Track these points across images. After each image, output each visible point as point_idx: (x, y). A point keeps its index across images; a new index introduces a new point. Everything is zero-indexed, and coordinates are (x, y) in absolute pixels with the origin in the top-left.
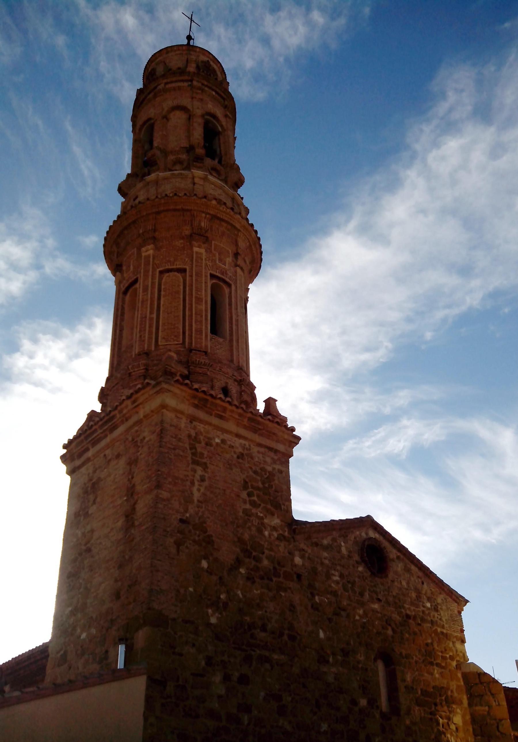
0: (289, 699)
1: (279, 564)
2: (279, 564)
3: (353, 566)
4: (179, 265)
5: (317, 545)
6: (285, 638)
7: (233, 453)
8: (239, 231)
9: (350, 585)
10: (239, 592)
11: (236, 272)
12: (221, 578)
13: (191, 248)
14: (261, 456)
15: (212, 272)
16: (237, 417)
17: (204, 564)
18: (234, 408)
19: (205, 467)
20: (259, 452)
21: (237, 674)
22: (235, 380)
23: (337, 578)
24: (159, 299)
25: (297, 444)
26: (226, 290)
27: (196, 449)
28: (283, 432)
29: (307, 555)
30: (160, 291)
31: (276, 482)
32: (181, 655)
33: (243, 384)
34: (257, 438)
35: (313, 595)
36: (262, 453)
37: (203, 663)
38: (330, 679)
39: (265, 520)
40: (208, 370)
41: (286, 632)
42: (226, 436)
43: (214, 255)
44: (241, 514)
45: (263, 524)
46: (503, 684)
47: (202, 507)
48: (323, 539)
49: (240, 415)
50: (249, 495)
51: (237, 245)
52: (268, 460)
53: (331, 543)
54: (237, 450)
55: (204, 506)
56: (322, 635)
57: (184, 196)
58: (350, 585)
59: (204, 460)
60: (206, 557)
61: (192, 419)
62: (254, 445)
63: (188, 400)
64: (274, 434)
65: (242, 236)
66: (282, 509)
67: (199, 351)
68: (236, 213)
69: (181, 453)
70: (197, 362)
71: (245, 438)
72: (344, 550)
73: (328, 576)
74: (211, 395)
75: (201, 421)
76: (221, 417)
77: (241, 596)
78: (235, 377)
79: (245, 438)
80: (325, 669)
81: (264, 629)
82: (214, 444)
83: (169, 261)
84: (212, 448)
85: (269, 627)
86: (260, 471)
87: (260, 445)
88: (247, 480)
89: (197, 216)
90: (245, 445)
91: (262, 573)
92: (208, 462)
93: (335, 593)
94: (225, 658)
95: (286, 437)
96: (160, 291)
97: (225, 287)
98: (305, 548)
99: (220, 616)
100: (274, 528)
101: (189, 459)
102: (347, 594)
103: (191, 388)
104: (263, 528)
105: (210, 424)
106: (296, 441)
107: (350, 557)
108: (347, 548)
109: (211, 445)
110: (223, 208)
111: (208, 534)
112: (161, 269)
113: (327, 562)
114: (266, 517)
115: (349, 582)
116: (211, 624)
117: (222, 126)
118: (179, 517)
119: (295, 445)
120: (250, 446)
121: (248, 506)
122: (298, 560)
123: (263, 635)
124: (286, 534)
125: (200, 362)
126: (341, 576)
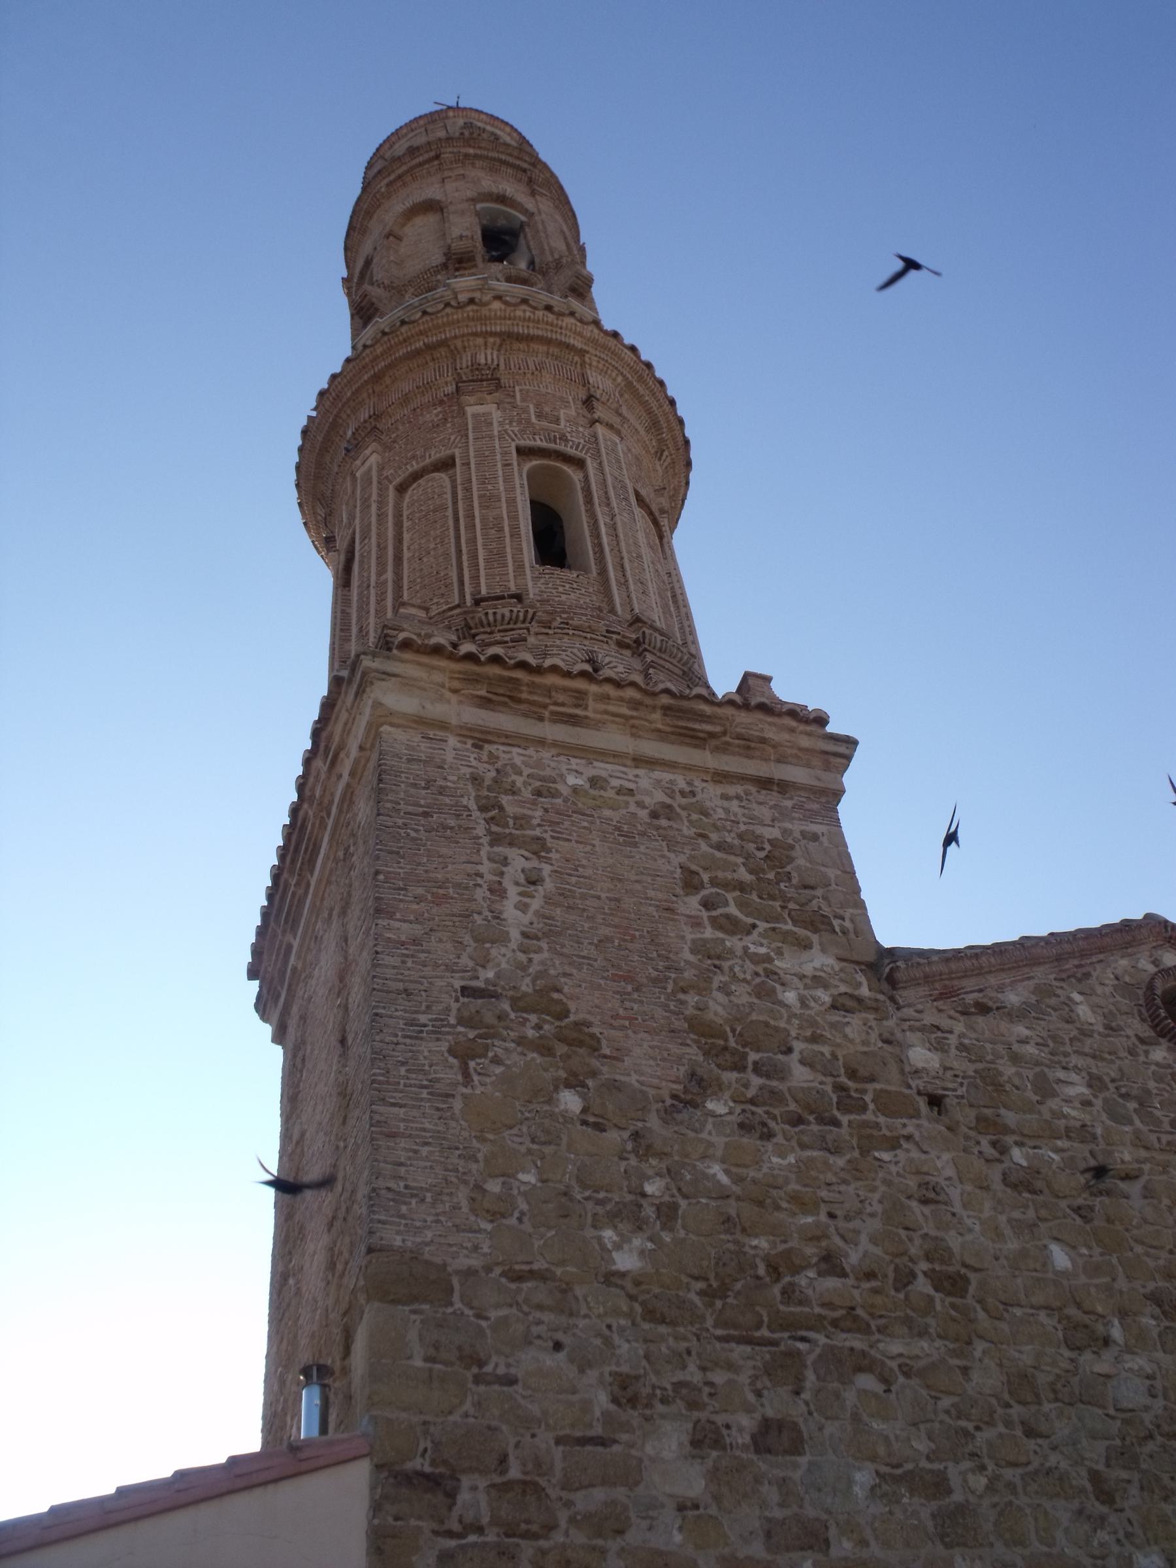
0: (979, 1482)
1: (852, 1074)
2: (852, 1074)
3: (1132, 1052)
4: (436, 455)
5: (983, 1009)
6: (922, 1285)
7: (633, 808)
8: (582, 353)
9: (1132, 1105)
10: (716, 1170)
11: (595, 436)
12: (636, 1136)
13: (462, 413)
14: (734, 805)
15: (522, 443)
16: (625, 711)
17: (570, 1101)
18: (608, 689)
19: (538, 848)
20: (725, 797)
21: (746, 1422)
22: (621, 645)
23: (1080, 1089)
24: (399, 540)
25: (848, 758)
26: (575, 476)
27: (501, 808)
28: (792, 730)
29: (953, 1040)
30: (398, 525)
31: (801, 862)
32: (511, 1381)
33: (645, 650)
34: (706, 758)
35: (1003, 1150)
36: (738, 797)
37: (602, 1399)
38: (1132, 1394)
39: (776, 962)
40: (528, 629)
41: (924, 1266)
42: (602, 769)
43: (525, 410)
44: (687, 955)
45: (770, 973)
46: (297, 1173)
47: (539, 950)
48: (1001, 989)
49: (635, 705)
50: (707, 904)
51: (585, 383)
52: (765, 813)
53: (1033, 999)
54: (647, 800)
55: (545, 946)
56: (1060, 1258)
57: (421, 317)
58: (1132, 1105)
59: (537, 832)
60: (574, 1082)
61: (480, 738)
62: (704, 781)
63: (455, 691)
64: (763, 741)
65: (594, 363)
66: (837, 929)
67: (502, 598)
68: (560, 314)
69: (452, 822)
70: (491, 618)
71: (671, 765)
72: (1084, 1012)
73: (1045, 1089)
74: (523, 665)
75: (511, 739)
76: (573, 721)
77: (724, 1179)
78: (615, 636)
79: (671, 765)
80: (1102, 1367)
81: (830, 1264)
82: (565, 791)
83: (414, 457)
84: (559, 801)
85: (853, 1258)
86: (737, 842)
87: (721, 777)
88: (694, 867)
89: (464, 348)
90: (671, 782)
91: (793, 1106)
92: (547, 836)
93: (1083, 1133)
94: (692, 1374)
95: (805, 742)
96: (398, 525)
97: (568, 469)
98: (945, 1023)
99: (650, 1245)
100: (818, 981)
101: (480, 830)
102: (1127, 1129)
103: (452, 657)
104: (778, 986)
105: (541, 742)
106: (842, 749)
107: (1111, 1029)
108: (1094, 1007)
109: (555, 794)
110: (524, 311)
111: (572, 1018)
112: (398, 480)
113: (1031, 1049)
114: (780, 953)
115: (1126, 1096)
116: (623, 1275)
117: (525, 212)
118: (458, 984)
119: (844, 761)
120: (689, 784)
121: (709, 933)
122: (920, 1055)
123: (831, 1283)
124: (864, 991)
125: (499, 617)
126: (1095, 1082)
